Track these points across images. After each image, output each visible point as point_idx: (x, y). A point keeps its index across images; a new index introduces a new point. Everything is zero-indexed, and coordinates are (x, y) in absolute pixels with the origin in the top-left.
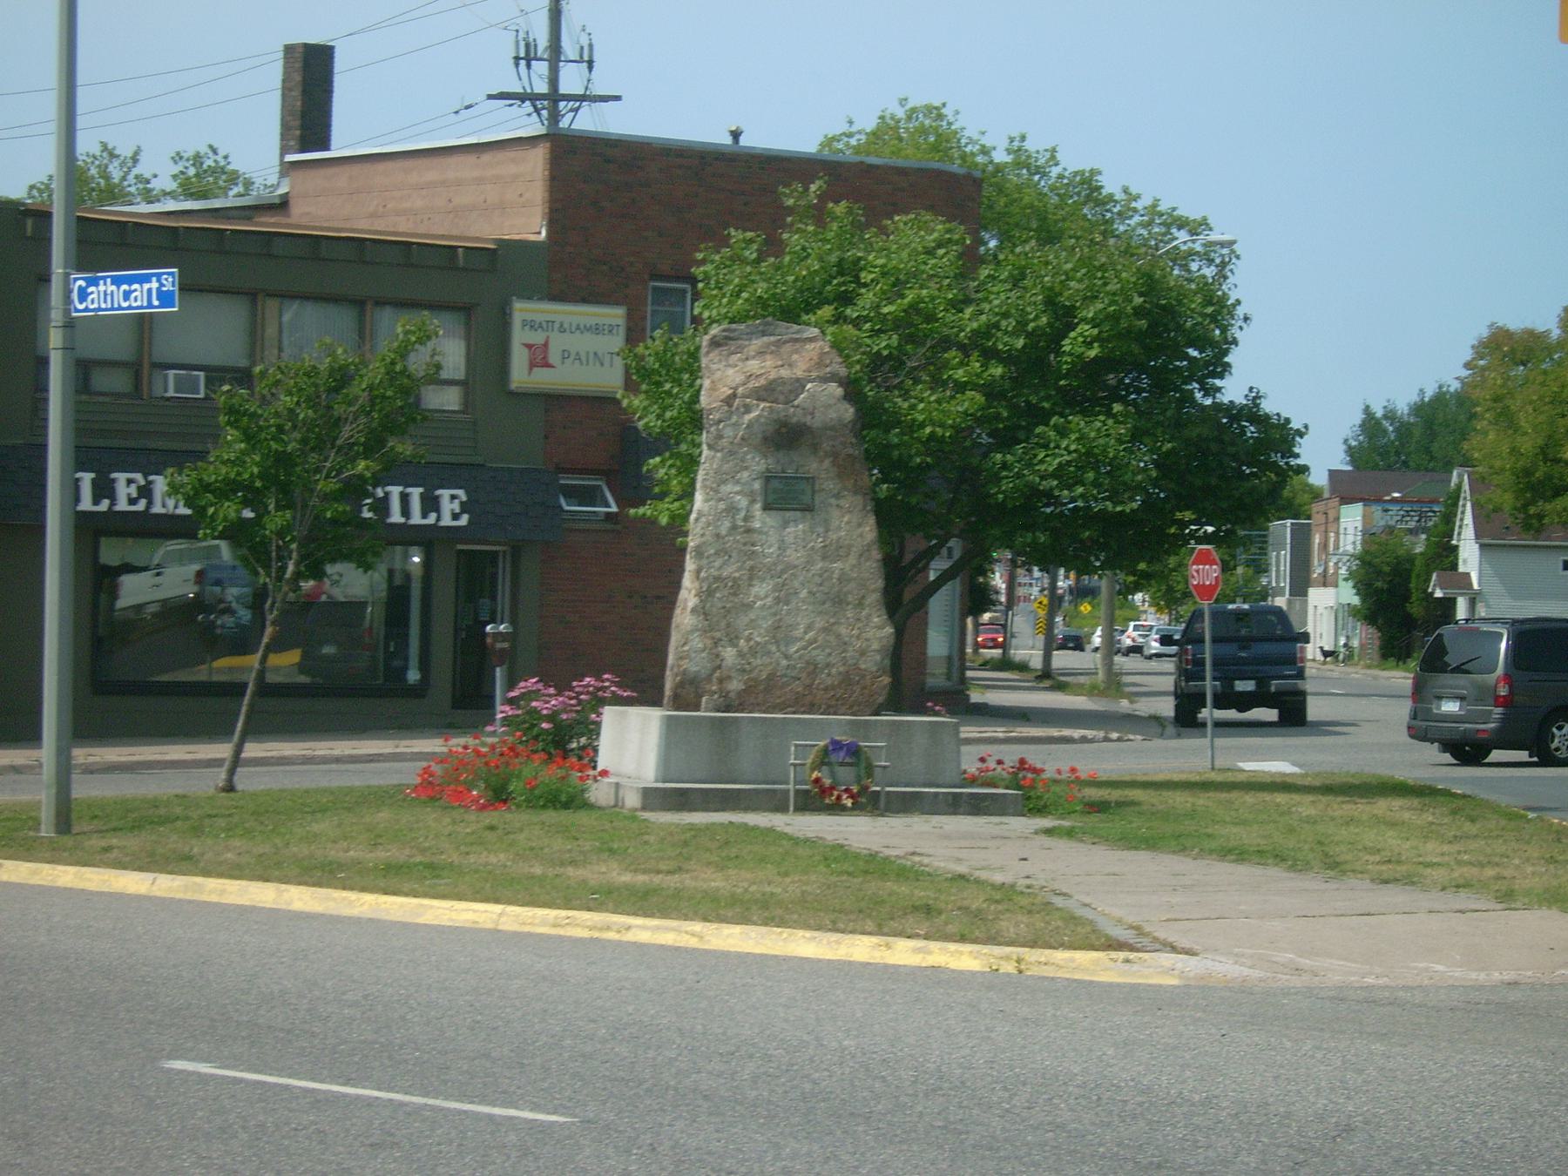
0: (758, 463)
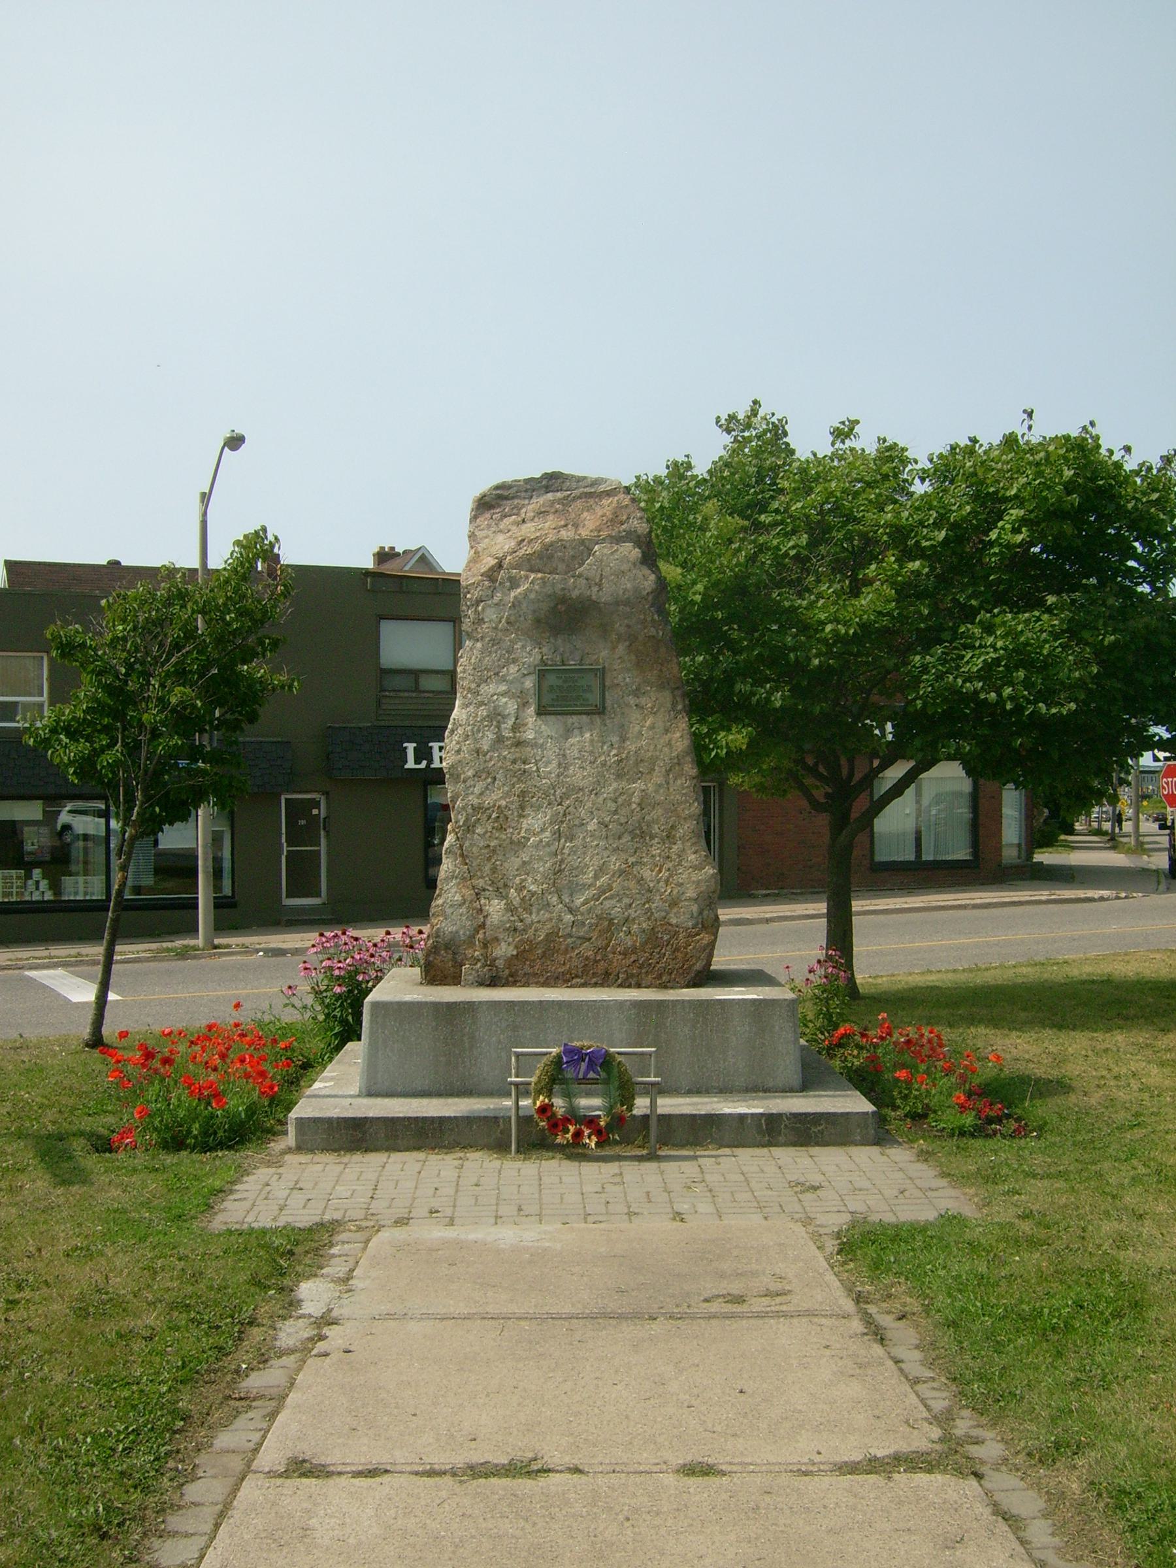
0: (529, 655)
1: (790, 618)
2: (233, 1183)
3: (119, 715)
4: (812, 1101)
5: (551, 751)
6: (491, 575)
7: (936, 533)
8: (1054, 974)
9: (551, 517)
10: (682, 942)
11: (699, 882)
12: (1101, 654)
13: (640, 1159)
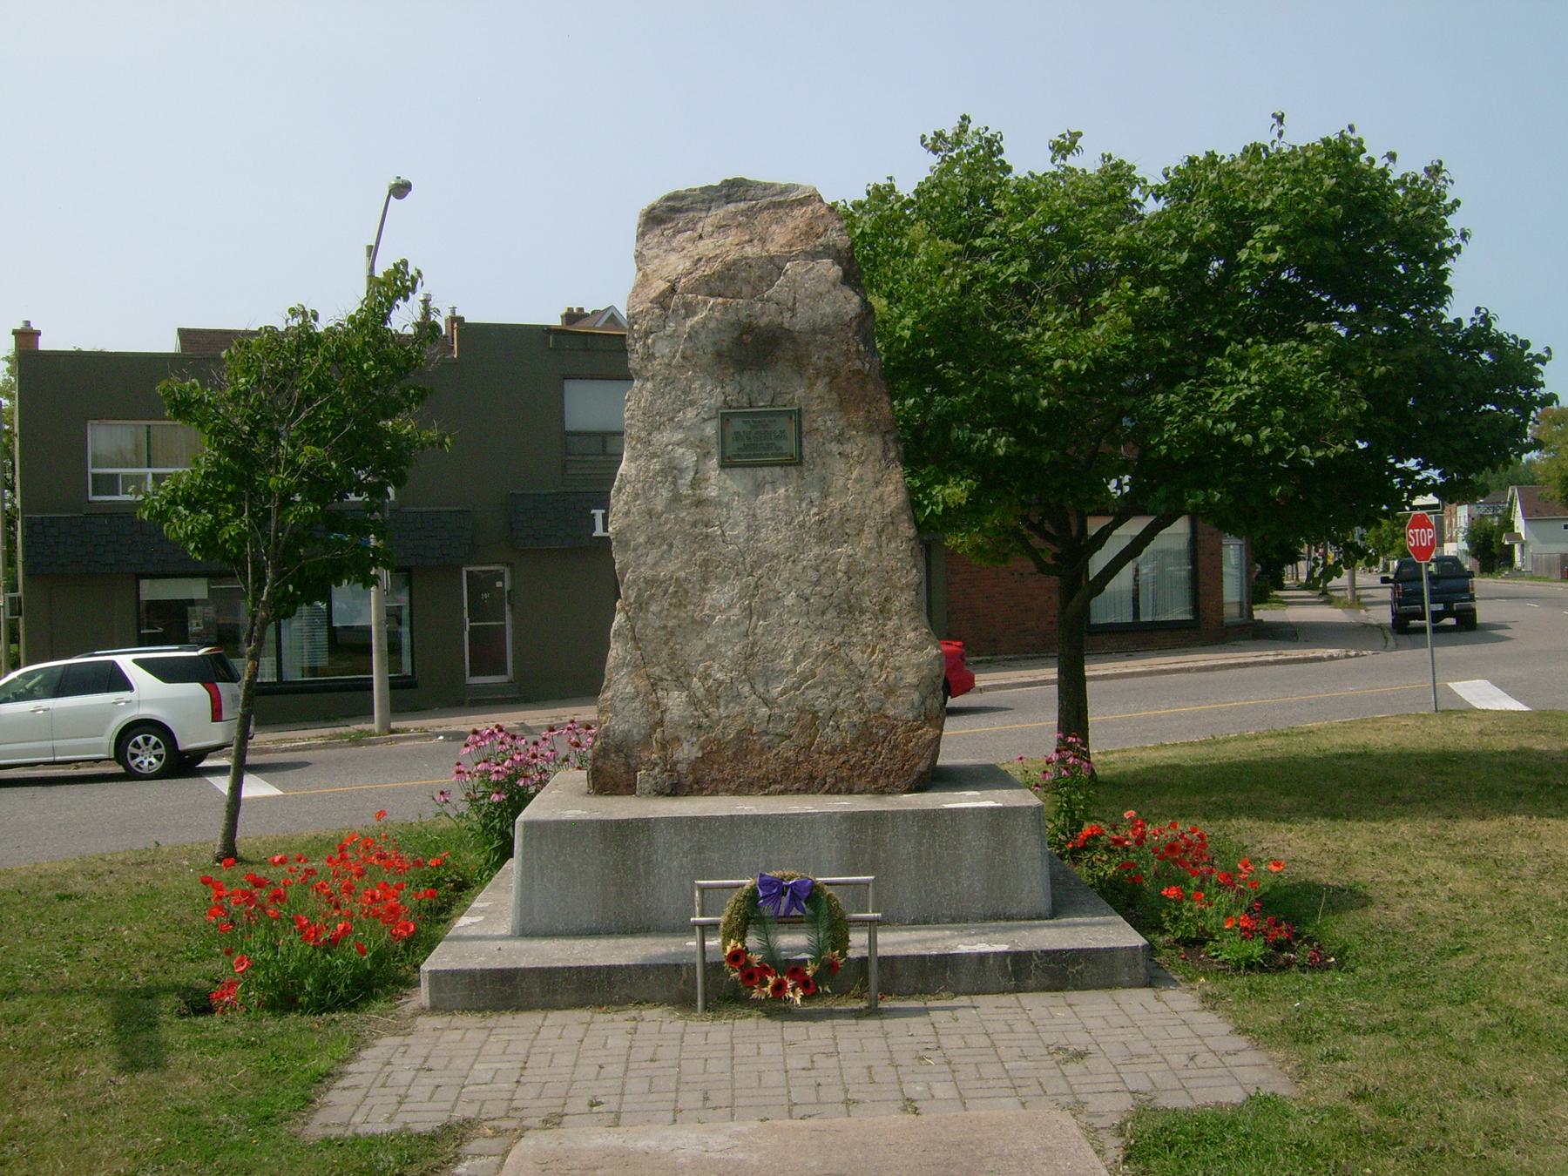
0: (710, 395)
1: (1012, 354)
2: (346, 1061)
3: (245, 481)
4: (1067, 932)
5: (739, 511)
6: (662, 301)
8: (1300, 747)
9: (734, 231)
10: (901, 738)
11: (919, 666)
12: (1370, 388)
13: (858, 1015)
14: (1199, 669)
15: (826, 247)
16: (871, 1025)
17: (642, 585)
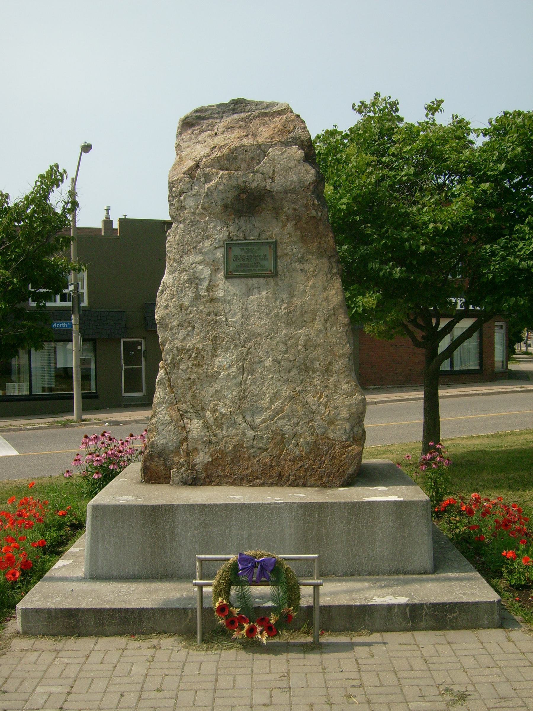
0: (219, 232)
1: (403, 220)
6: (191, 173)
7: (499, 165)
9: (236, 131)
11: (351, 405)
13: (306, 648)
14: (484, 394)
15: (294, 139)
16: (314, 658)
17: (176, 352)
